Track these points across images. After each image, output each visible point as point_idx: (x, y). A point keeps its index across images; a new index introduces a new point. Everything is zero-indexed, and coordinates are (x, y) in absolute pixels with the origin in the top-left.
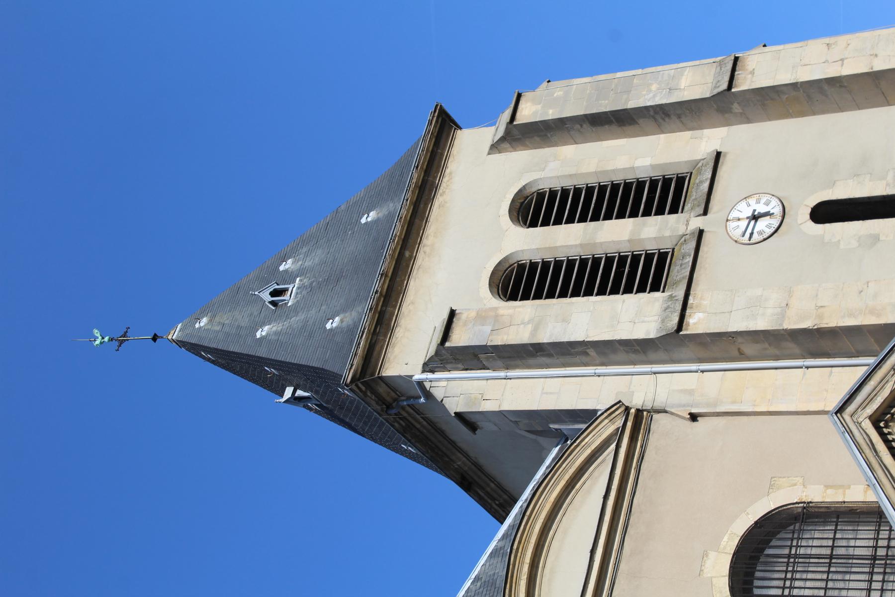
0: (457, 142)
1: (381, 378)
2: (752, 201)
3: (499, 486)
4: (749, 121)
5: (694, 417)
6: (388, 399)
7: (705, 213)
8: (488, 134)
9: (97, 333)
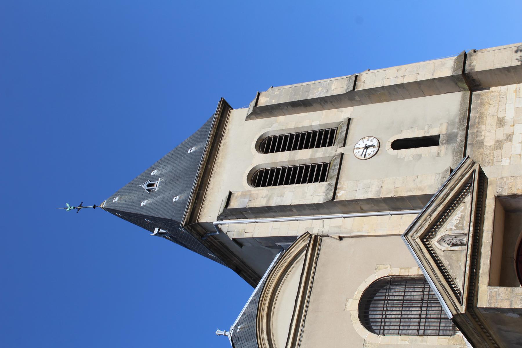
0: (231, 115)
1: (199, 224)
2: (365, 140)
3: (254, 272)
4: (363, 104)
5: (341, 238)
6: (202, 233)
7: (344, 146)
8: (245, 112)
9: (68, 205)
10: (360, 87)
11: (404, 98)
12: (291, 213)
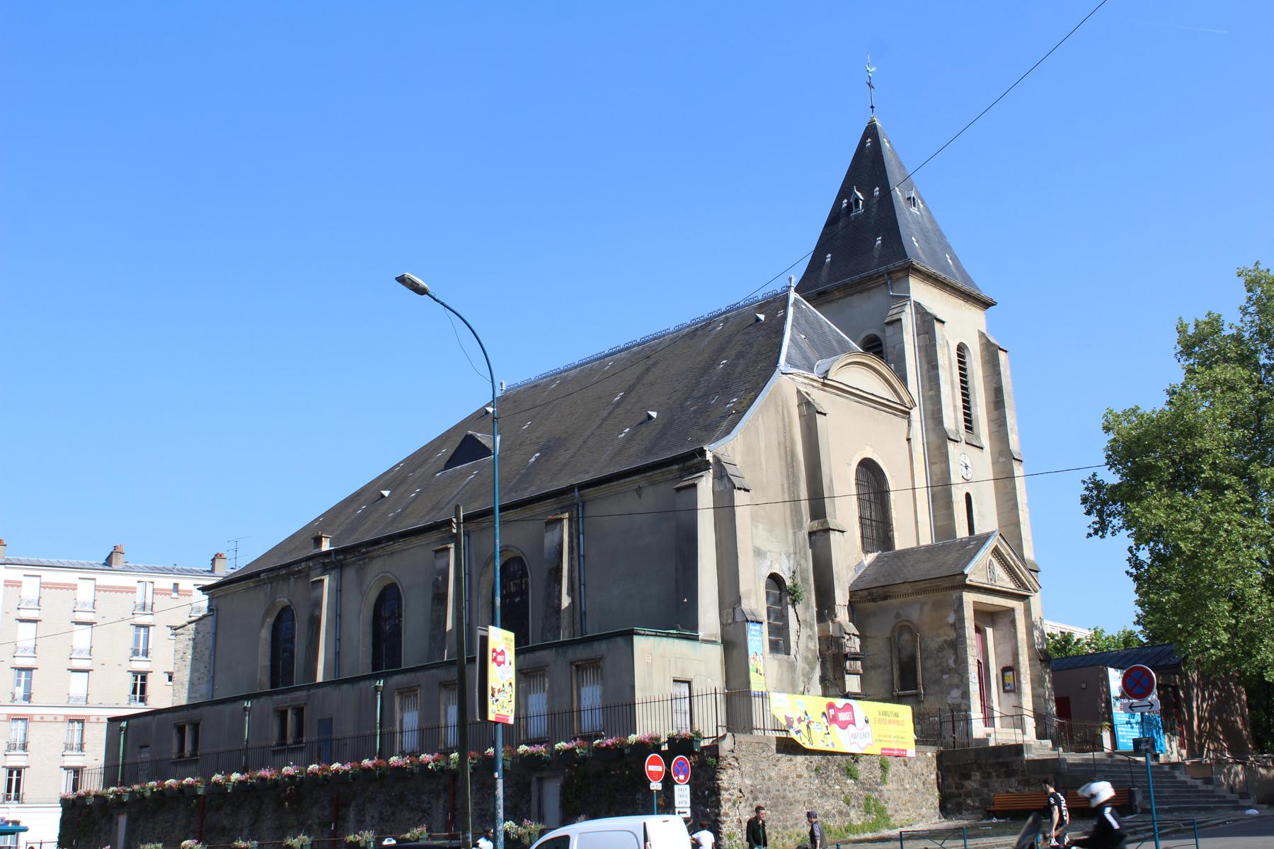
4: (993, 463)
5: (909, 440)
9: (874, 69)
10: (951, 445)
11: (998, 506)
12: (927, 388)
